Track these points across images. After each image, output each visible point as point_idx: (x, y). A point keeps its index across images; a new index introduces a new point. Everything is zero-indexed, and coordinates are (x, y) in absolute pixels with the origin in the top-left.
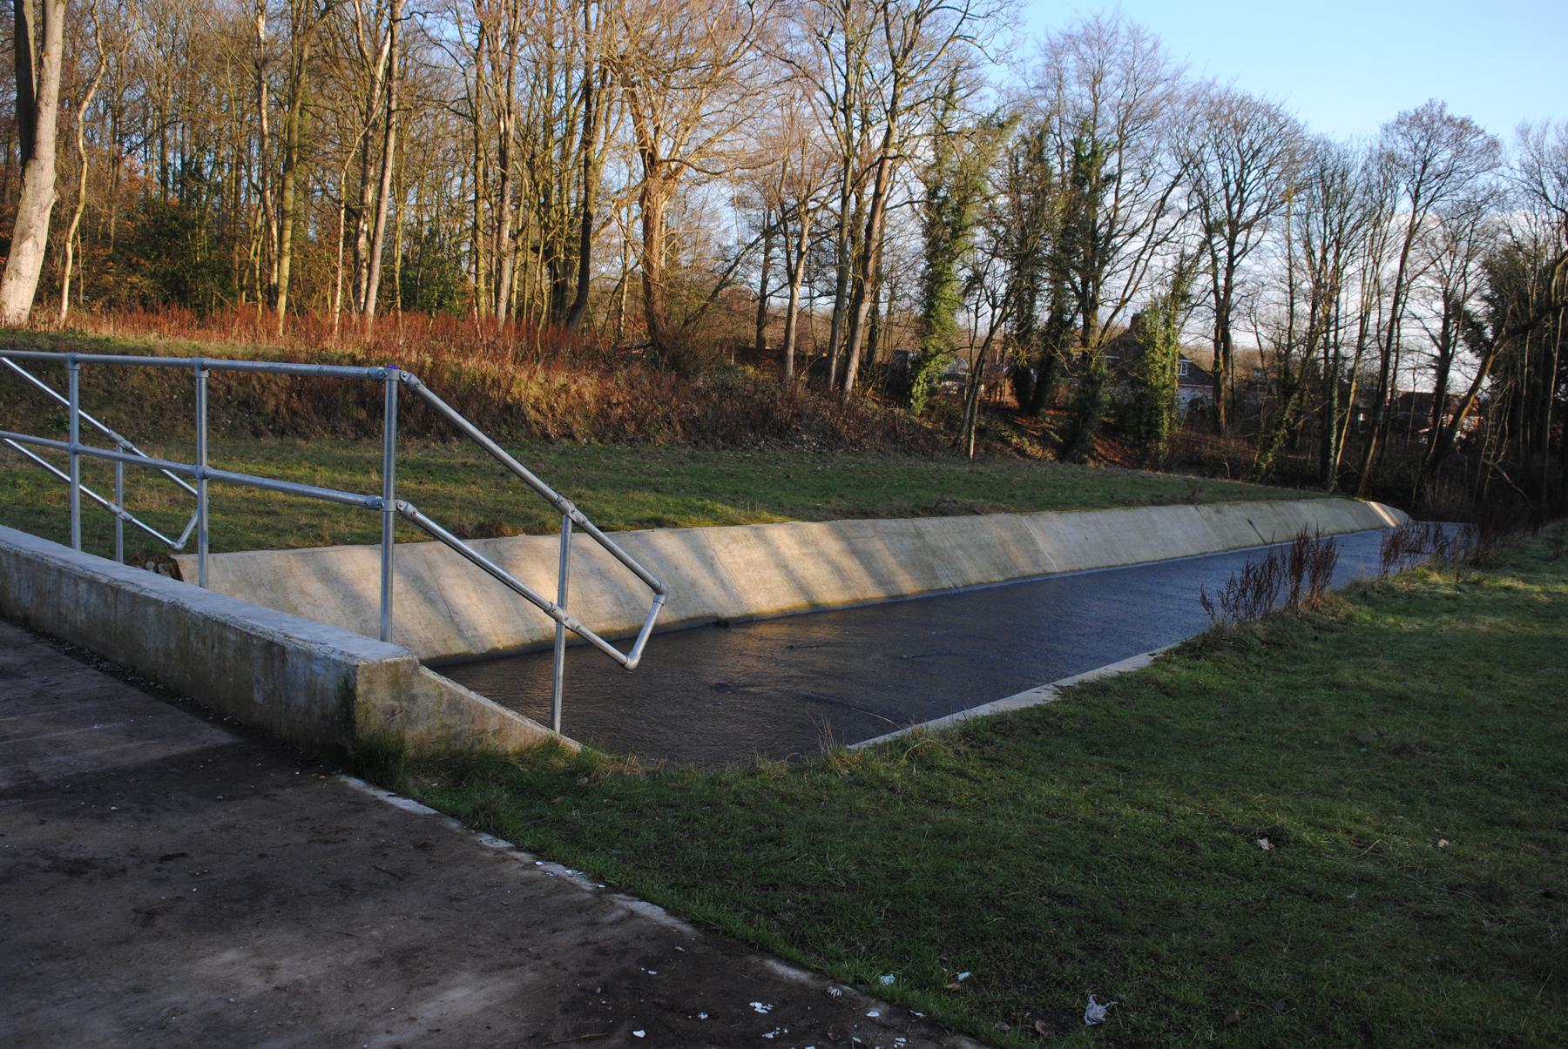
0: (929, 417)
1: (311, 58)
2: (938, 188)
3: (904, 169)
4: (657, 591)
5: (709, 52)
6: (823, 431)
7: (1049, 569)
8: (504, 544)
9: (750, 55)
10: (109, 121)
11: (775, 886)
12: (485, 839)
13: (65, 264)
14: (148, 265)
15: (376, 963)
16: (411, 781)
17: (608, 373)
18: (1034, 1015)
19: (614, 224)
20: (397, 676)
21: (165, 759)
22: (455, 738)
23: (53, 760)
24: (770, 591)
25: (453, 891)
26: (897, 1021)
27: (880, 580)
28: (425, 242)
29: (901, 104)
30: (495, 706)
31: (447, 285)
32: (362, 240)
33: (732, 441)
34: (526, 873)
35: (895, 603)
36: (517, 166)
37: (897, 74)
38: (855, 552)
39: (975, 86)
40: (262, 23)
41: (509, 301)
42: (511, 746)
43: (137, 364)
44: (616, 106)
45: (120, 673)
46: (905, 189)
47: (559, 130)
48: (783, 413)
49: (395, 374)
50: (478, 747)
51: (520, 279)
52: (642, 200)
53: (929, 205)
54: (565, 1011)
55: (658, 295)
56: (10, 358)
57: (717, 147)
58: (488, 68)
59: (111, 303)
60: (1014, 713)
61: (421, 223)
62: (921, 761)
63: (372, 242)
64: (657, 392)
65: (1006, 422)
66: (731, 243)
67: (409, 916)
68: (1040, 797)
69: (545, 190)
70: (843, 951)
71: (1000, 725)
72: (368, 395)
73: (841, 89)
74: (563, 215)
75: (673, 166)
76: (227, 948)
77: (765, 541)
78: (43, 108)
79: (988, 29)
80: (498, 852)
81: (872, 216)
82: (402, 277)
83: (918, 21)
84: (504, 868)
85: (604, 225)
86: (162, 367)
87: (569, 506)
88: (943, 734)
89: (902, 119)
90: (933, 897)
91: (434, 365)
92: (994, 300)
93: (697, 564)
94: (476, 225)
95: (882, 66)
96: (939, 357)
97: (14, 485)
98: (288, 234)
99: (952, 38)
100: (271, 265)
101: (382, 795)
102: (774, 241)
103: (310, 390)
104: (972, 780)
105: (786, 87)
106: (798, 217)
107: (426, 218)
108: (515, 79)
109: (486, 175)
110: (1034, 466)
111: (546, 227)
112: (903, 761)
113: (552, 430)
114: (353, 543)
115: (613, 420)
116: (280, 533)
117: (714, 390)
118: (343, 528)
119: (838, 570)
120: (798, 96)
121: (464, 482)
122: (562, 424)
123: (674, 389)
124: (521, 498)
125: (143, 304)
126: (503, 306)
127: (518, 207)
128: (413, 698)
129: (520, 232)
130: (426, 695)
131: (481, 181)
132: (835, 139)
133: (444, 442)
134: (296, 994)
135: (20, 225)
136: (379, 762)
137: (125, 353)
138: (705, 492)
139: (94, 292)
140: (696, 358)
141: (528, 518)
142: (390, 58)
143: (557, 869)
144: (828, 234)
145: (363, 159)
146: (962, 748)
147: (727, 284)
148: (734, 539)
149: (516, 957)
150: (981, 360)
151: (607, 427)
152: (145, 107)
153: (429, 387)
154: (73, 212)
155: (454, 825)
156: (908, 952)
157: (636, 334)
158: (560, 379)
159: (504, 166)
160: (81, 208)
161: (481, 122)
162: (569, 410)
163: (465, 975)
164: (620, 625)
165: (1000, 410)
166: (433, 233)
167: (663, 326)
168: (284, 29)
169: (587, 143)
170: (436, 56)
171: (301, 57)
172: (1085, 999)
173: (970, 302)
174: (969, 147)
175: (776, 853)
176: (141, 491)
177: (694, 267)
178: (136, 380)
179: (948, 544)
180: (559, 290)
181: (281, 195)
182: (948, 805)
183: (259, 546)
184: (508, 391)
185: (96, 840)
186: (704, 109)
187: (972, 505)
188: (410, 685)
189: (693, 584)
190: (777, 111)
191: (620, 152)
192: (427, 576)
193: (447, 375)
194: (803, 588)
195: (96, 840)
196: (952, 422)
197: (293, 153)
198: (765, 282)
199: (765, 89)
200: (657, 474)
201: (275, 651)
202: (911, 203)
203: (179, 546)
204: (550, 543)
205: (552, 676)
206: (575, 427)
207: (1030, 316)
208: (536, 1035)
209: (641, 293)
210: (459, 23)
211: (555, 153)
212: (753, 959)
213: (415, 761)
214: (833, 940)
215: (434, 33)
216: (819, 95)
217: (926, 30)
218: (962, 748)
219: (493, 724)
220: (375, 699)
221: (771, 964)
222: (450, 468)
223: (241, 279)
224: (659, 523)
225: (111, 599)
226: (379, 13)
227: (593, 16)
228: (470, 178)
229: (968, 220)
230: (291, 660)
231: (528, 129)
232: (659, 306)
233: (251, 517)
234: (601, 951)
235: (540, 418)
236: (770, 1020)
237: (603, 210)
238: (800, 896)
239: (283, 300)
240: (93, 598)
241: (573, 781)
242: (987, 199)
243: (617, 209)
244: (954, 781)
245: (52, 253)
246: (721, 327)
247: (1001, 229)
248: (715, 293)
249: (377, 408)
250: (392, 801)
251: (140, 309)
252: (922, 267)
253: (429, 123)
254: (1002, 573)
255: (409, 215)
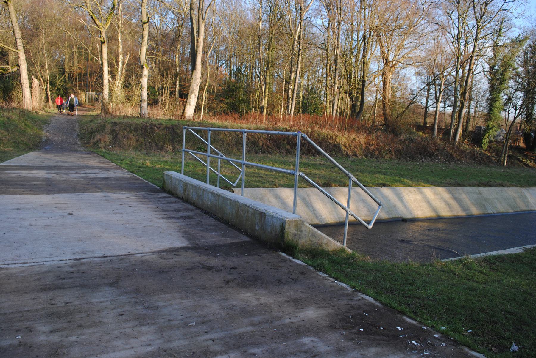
0: (489, 151)
1: (275, 34)
2: (494, 66)
3: (481, 60)
4: (379, 204)
5: (408, 23)
6: (447, 155)
7: (533, 209)
8: (332, 189)
9: (423, 22)
10: (215, 56)
11: (409, 297)
12: (320, 273)
13: (202, 101)
14: (226, 101)
15: (288, 301)
16: (300, 256)
17: (369, 134)
18: (493, 346)
19: (373, 83)
20: (297, 224)
21: (231, 243)
22: (313, 244)
23: (202, 241)
24: (422, 210)
25: (310, 286)
26: (443, 339)
27: (464, 209)
28: (310, 91)
29: (480, 36)
30: (326, 236)
31: (316, 105)
32: (290, 91)
33: (413, 158)
34: (332, 284)
35: (470, 217)
36: (340, 65)
37: (478, 25)
38: (455, 198)
39: (510, 27)
40: (261, 24)
41: (337, 110)
42: (330, 249)
43: (222, 131)
44: (375, 43)
45: (218, 219)
46: (481, 67)
47: (355, 52)
48: (431, 149)
49: (300, 134)
50: (320, 248)
51: (341, 103)
52: (383, 75)
53: (491, 73)
54: (340, 321)
55: (387, 107)
56: (192, 129)
57: (410, 55)
58: (331, 33)
59: (215, 112)
60: (505, 255)
61: (309, 85)
62: (467, 267)
63: (293, 92)
64: (386, 141)
65: (520, 153)
66: (415, 88)
67: (297, 291)
68: (509, 282)
69: (349, 73)
70: (429, 318)
71: (499, 258)
72: (291, 141)
73: (456, 32)
74: (355, 81)
75: (394, 63)
76: (247, 292)
77: (422, 193)
78: (198, 55)
79: (515, 6)
80: (324, 277)
81: (468, 77)
82: (302, 103)
83: (486, 5)
84: (325, 282)
85: (370, 84)
86: (229, 132)
87: (351, 176)
88: (477, 259)
89: (479, 42)
90: (463, 307)
91: (312, 132)
92: (516, 107)
93: (397, 199)
94: (326, 86)
95: (472, 23)
96: (494, 129)
97: (189, 166)
98: (267, 90)
99: (500, 10)
100: (262, 100)
101: (291, 258)
102: (431, 87)
103: (273, 139)
104: (484, 274)
105: (436, 33)
106: (439, 79)
107: (310, 83)
108: (340, 36)
109: (330, 68)
110: (530, 170)
111: (350, 85)
112: (461, 266)
113: (350, 154)
114: (285, 187)
115: (371, 150)
116: (263, 183)
117: (407, 140)
118: (282, 182)
119: (448, 204)
120: (440, 35)
121: (320, 169)
122: (353, 151)
123: (392, 140)
124: (338, 175)
125: (224, 113)
126: (335, 112)
127: (340, 79)
128: (301, 231)
129: (341, 87)
130: (305, 231)
131: (328, 71)
132: (454, 50)
133: (314, 156)
134: (265, 306)
135: (191, 89)
136: (290, 249)
137: (219, 128)
138: (401, 175)
139: (210, 109)
140: (400, 129)
141: (340, 182)
142: (300, 32)
143: (341, 284)
144: (451, 84)
145: (291, 65)
146: (483, 264)
147: (413, 103)
148: (410, 192)
149: (327, 305)
150: (510, 130)
151: (368, 152)
152: (225, 52)
153: (310, 138)
154: (205, 85)
155: (312, 268)
156: (452, 322)
157: (379, 121)
158: (353, 136)
159: (336, 65)
160: (207, 84)
161: (329, 51)
162: (356, 147)
163: (312, 308)
164: (368, 218)
165: (518, 149)
166: (312, 88)
167: (389, 118)
168: (267, 25)
169: (364, 56)
170: (314, 30)
171: (272, 33)
172: (512, 344)
173: (507, 108)
174: (506, 51)
175: (411, 288)
176: (223, 169)
177: (402, 97)
178: (222, 136)
179: (491, 197)
180: (353, 106)
181: (265, 78)
182: (474, 281)
183: (257, 187)
184: (335, 140)
185: (213, 262)
186: (405, 42)
187: (502, 183)
188: (301, 227)
189: (395, 206)
190: (433, 41)
191: (376, 59)
192: (307, 198)
193: (316, 135)
194: (434, 210)
195: (213, 262)
196: (498, 153)
197: (269, 64)
198: (427, 102)
199: (427, 34)
200: (385, 169)
201: (262, 215)
202: (484, 72)
203: (234, 185)
204: (346, 190)
205: (345, 230)
206: (357, 152)
207: (531, 113)
208: (331, 326)
209: (382, 107)
210: (322, 19)
211: (353, 60)
212: (399, 316)
213: (301, 250)
214: (427, 314)
215: (314, 23)
216: (448, 34)
217: (489, 8)
218: (483, 264)
219: (325, 241)
220: (290, 231)
221: (405, 318)
222: (316, 165)
223: (253, 104)
224: (384, 185)
225: (217, 198)
226: (296, 18)
227: (367, 13)
228: (325, 69)
229: (506, 77)
230: (267, 217)
231: (344, 53)
232: (388, 111)
233: (255, 178)
234: (352, 307)
235: (346, 149)
236: (402, 333)
237: (369, 78)
238: (417, 301)
239: (265, 111)
240: (213, 198)
241: (349, 260)
242: (514, 69)
243: (374, 79)
244: (477, 274)
245: (199, 97)
246: (411, 118)
247: (520, 80)
248: (408, 106)
249: (294, 145)
250: (294, 260)
251: (223, 114)
252: (488, 95)
253: (312, 52)
254: (513, 209)
255: (305, 82)
